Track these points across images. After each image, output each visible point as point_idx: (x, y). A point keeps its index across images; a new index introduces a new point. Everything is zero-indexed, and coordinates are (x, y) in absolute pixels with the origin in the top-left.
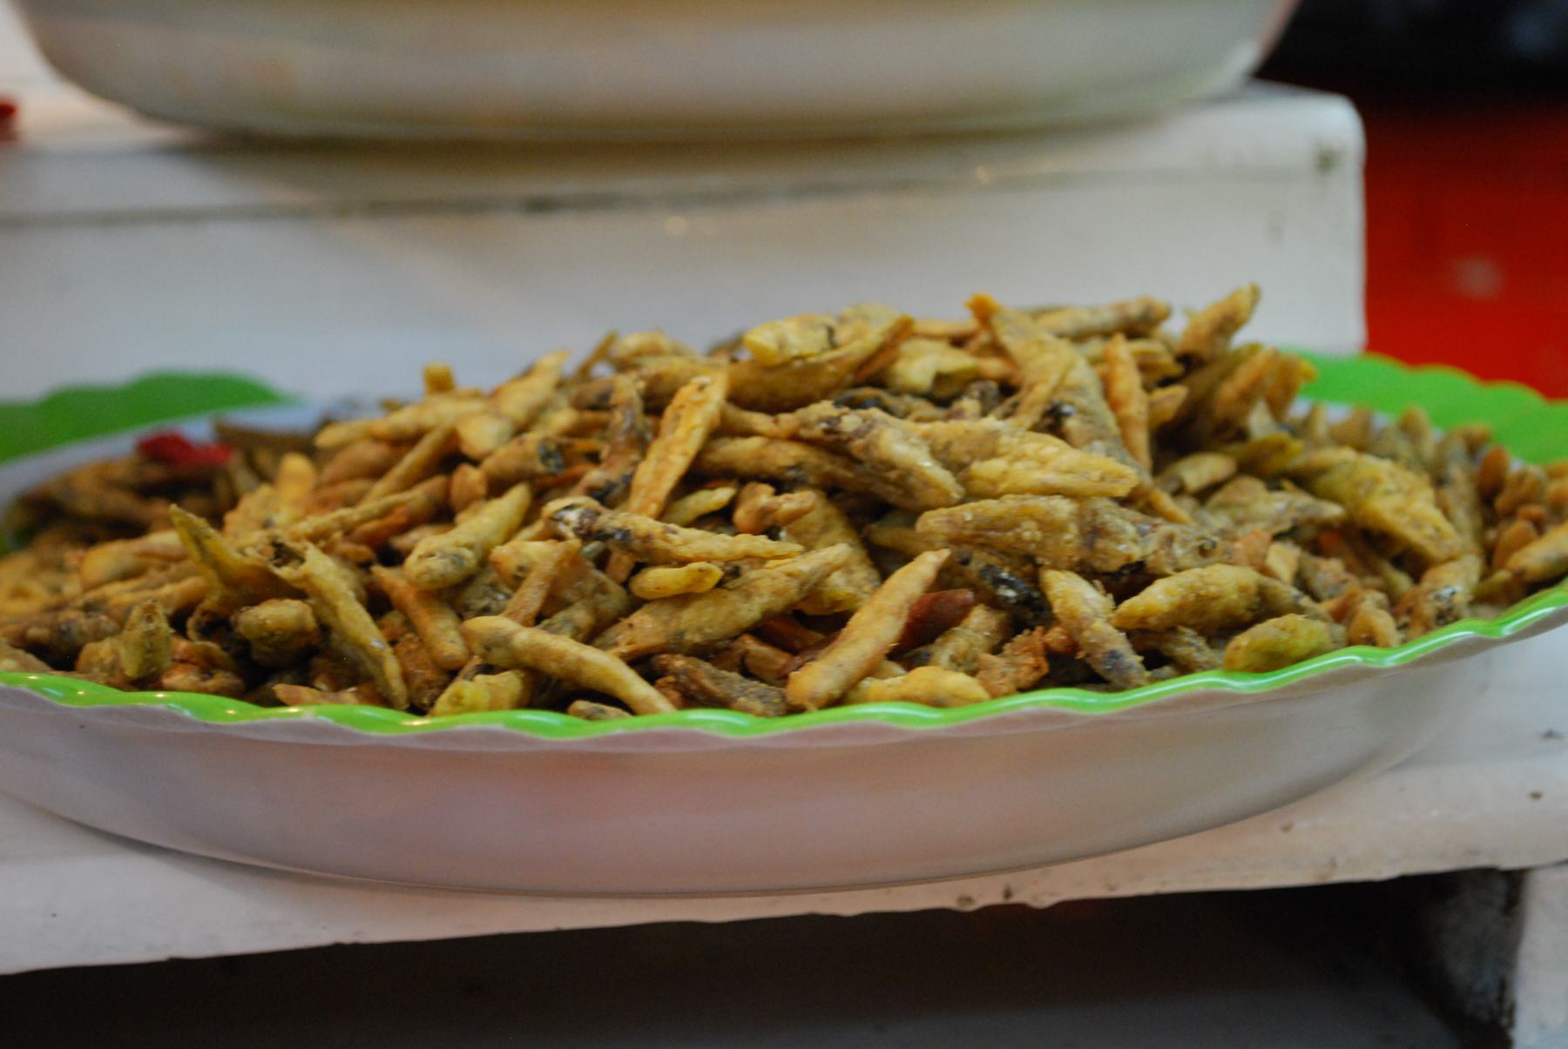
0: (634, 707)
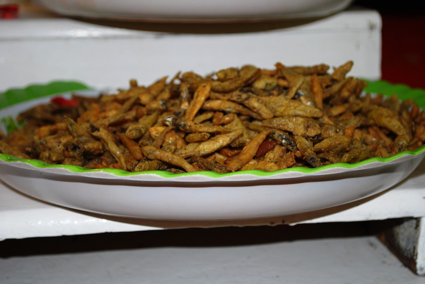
0: (187, 170)
